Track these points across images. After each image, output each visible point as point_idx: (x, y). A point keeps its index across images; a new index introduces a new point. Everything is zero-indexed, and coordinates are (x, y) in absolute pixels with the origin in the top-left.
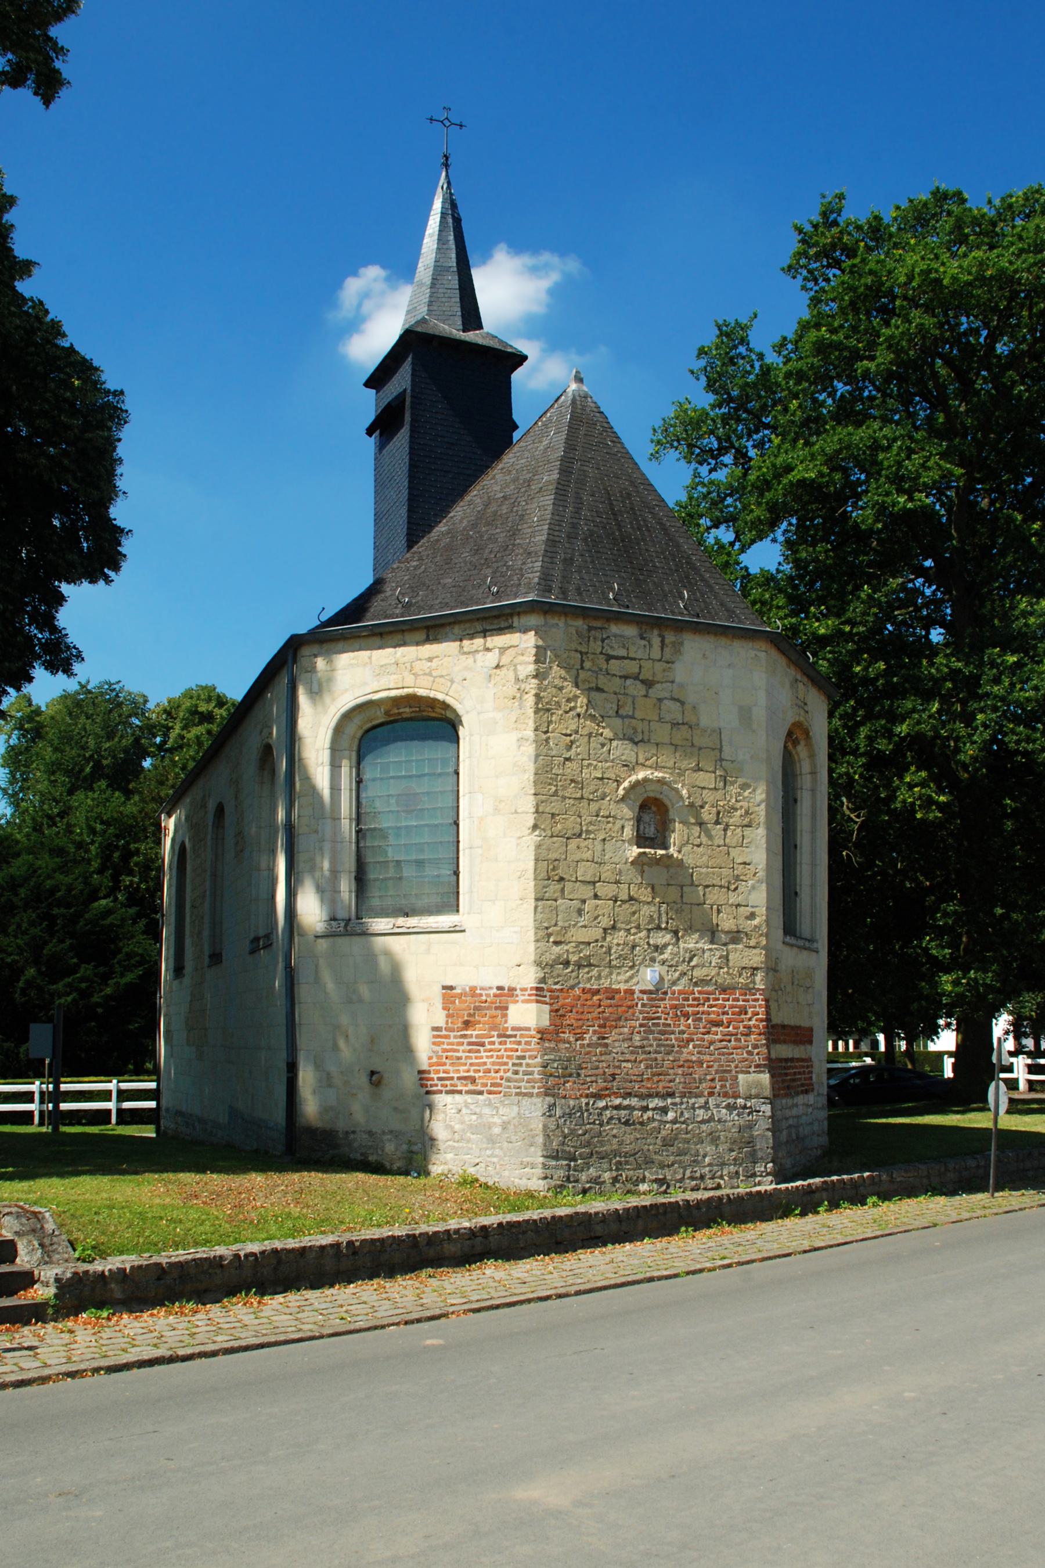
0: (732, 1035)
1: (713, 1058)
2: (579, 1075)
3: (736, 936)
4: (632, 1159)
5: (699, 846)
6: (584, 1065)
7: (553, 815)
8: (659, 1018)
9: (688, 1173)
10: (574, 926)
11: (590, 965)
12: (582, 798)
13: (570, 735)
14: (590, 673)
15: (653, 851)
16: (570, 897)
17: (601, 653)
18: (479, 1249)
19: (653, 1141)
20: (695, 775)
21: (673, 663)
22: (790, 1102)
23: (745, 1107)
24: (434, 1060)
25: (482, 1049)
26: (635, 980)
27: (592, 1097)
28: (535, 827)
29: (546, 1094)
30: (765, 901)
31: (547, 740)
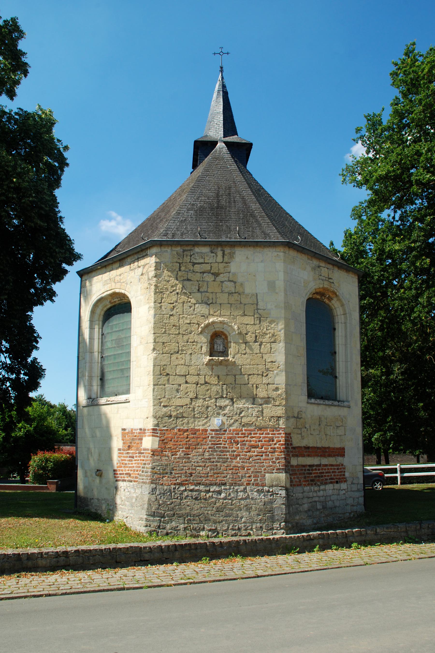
0: (264, 453)
1: (251, 465)
2: (171, 473)
3: (267, 400)
4: (197, 518)
5: (245, 354)
6: (175, 468)
7: (163, 343)
8: (221, 444)
9: (231, 527)
10: (174, 397)
11: (183, 417)
12: (179, 334)
13: (173, 303)
14: (184, 272)
15: (217, 358)
16: (173, 383)
17: (190, 262)
18: (62, 563)
19: (211, 509)
20: (242, 318)
21: (229, 263)
22: (316, 488)
23: (269, 491)
24: (119, 465)
25: (133, 459)
26: (208, 424)
27: (178, 485)
28: (154, 349)
29: (152, 483)
30: (285, 381)
31: (161, 307)
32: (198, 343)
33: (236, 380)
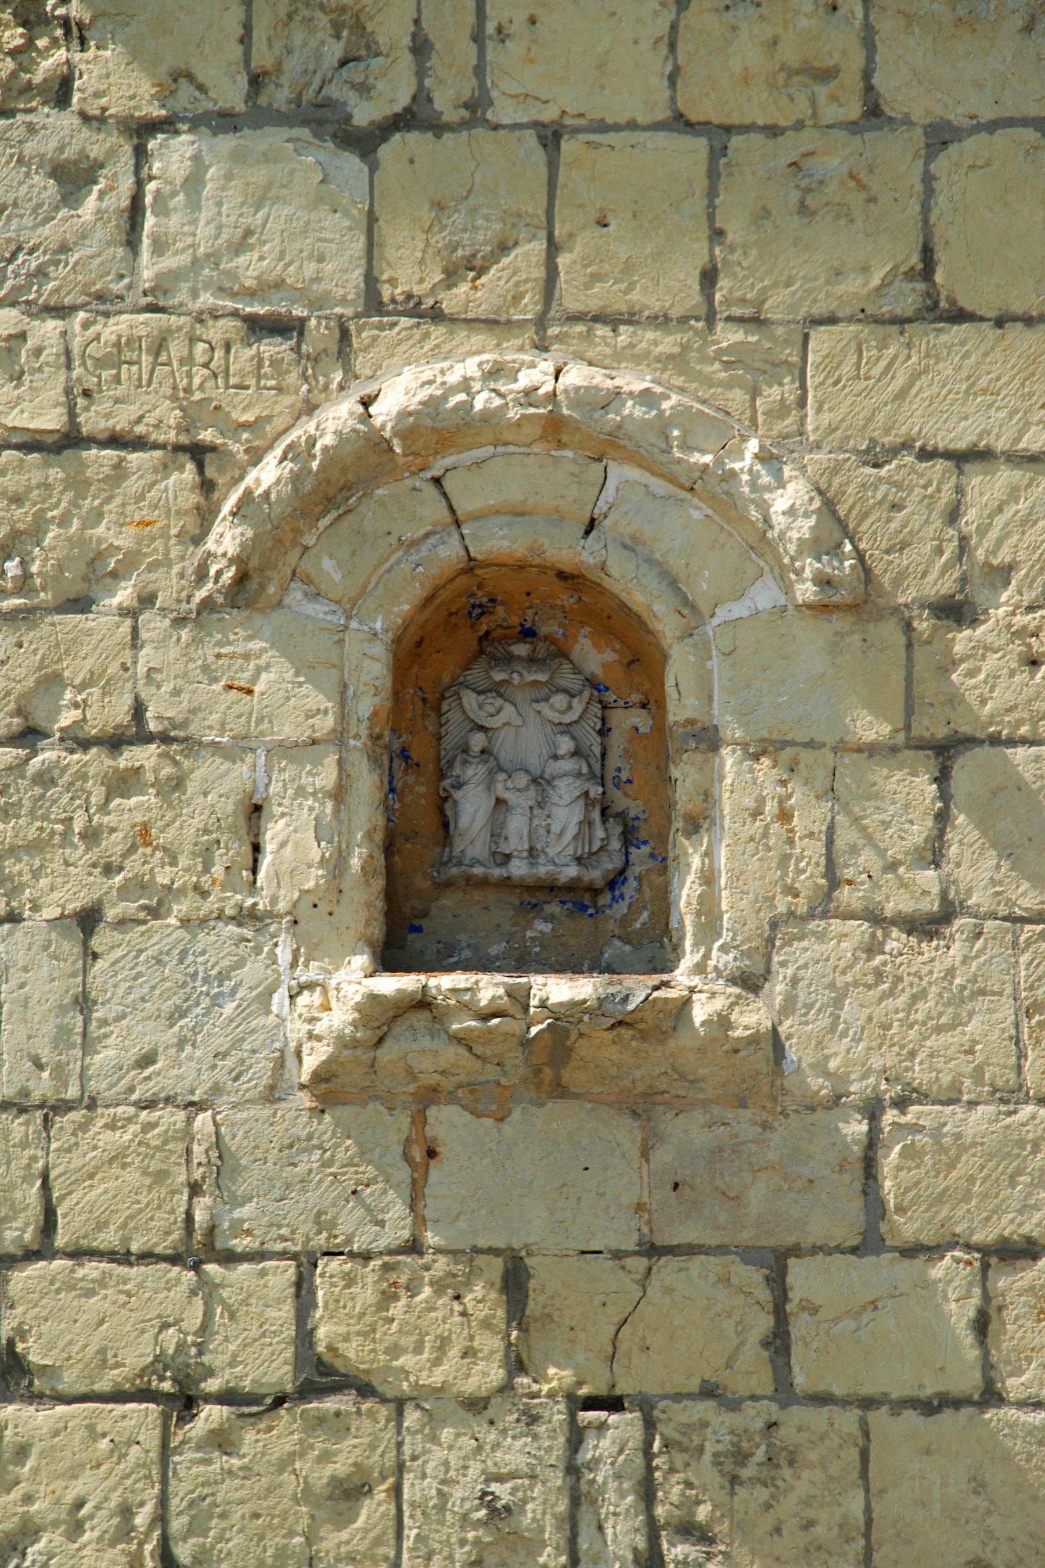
32: (192, 745)
33: (800, 1327)
